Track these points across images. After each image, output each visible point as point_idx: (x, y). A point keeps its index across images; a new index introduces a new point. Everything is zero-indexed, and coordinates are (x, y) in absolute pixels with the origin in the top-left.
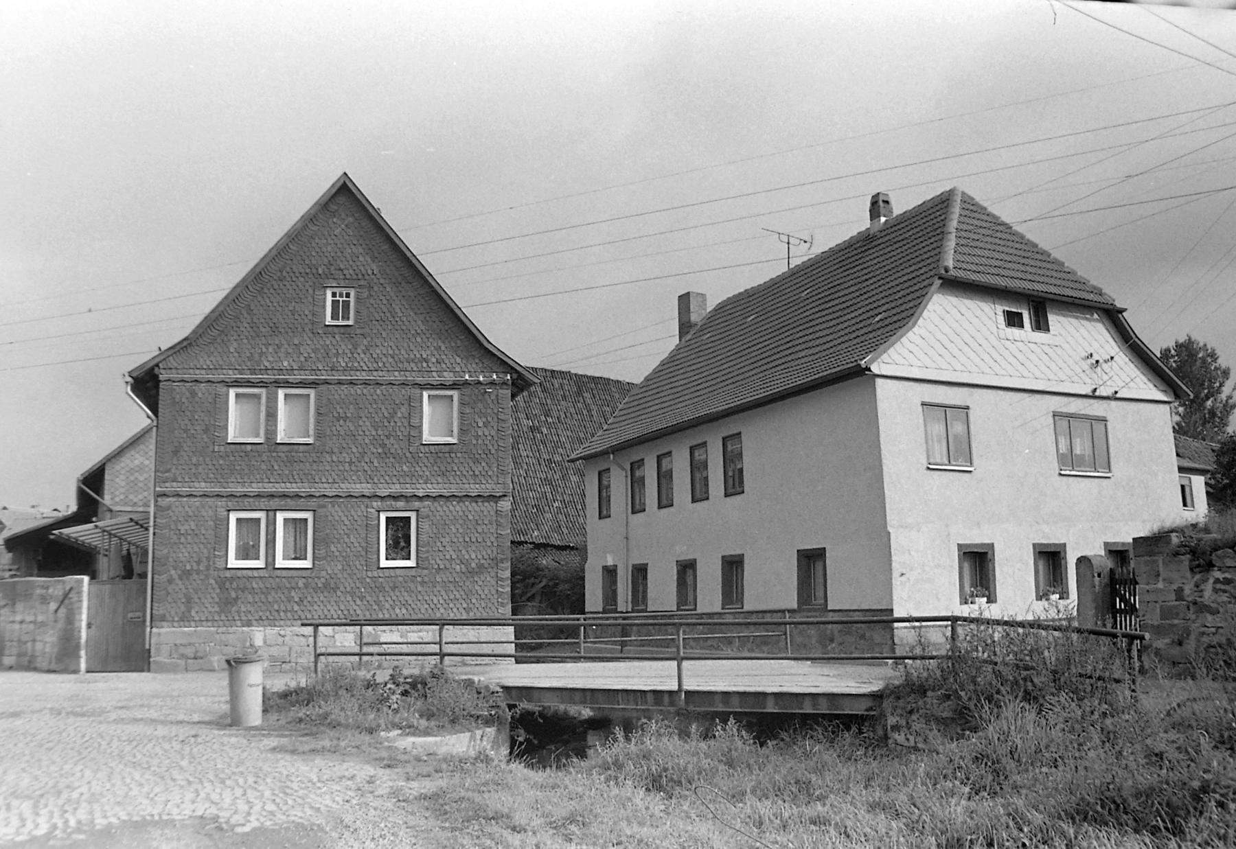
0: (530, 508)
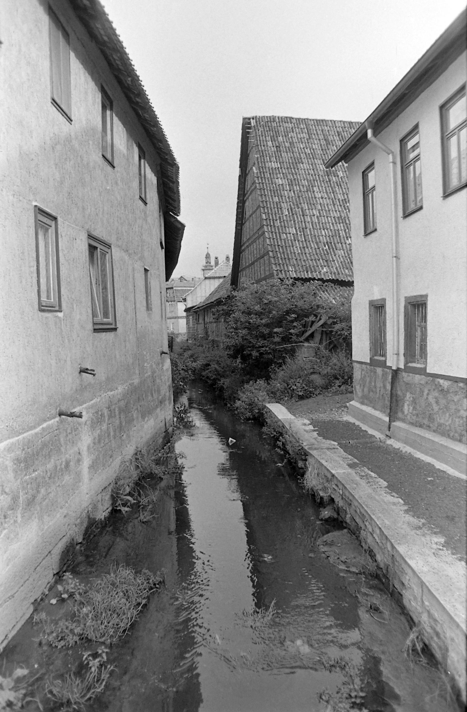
0: (321, 245)
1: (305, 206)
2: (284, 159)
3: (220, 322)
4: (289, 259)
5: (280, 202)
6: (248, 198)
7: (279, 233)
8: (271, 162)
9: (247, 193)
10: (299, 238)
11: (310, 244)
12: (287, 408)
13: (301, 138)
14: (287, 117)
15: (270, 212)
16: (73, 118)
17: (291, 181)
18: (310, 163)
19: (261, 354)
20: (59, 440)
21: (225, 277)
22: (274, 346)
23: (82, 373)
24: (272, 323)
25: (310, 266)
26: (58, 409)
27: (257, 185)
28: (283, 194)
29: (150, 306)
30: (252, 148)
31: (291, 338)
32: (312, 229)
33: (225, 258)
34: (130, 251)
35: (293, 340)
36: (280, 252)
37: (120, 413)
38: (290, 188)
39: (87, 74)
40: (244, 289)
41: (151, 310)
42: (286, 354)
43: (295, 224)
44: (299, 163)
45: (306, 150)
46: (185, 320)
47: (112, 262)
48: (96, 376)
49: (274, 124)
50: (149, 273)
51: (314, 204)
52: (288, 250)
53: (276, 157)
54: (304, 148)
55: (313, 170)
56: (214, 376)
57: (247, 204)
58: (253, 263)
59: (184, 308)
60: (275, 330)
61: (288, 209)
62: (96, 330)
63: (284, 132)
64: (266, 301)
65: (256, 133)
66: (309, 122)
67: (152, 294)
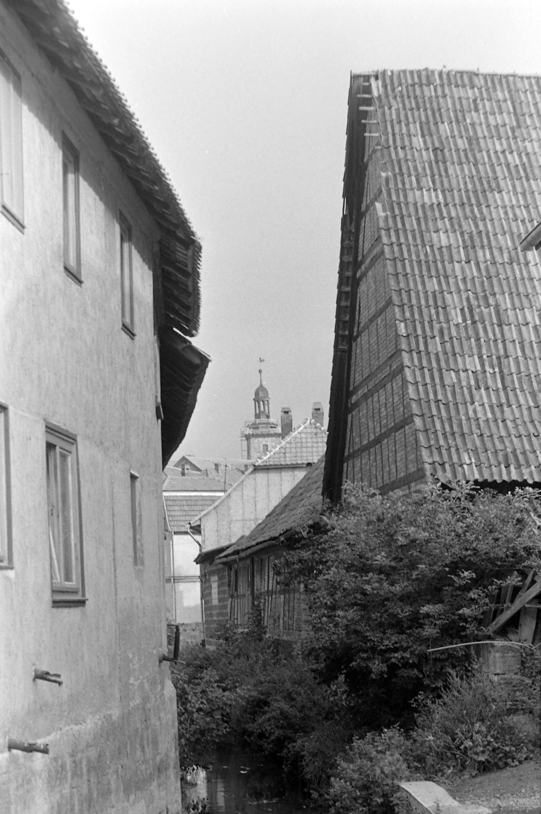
1: (506, 302)
2: (454, 181)
3: (295, 591)
4: (463, 435)
5: (442, 292)
6: (364, 274)
7: (440, 370)
8: (421, 189)
9: (362, 262)
10: (490, 383)
11: (516, 396)
12: (448, 790)
13: (497, 126)
14: (462, 73)
15: (417, 316)
16: (26, 224)
17: (471, 237)
18: (519, 190)
19: (393, 668)
20: (8, 791)
21: (309, 464)
22: (423, 647)
23: (40, 682)
24: (419, 593)
25: (514, 452)
26: (7, 737)
27: (387, 249)
28: (449, 272)
29: (139, 554)
30: (374, 151)
31: (464, 629)
32: (521, 359)
33: (311, 411)
34: (107, 444)
35: (468, 632)
36: (441, 418)
37: (89, 771)
38: (467, 255)
39: (42, 127)
40: (350, 509)
41: (142, 563)
42: (454, 667)
43: (479, 347)
44: (492, 191)
45: (509, 157)
46: (197, 587)
47: (78, 470)
48: (64, 685)
49: (429, 92)
50: (138, 484)
51: (527, 296)
52: (462, 412)
53: (433, 176)
54: (503, 152)
55: (527, 207)
56: (278, 733)
57: (363, 288)
58: (378, 441)
59: (196, 553)
60: (425, 609)
61: (462, 310)
62: (56, 604)
63: (455, 111)
64: (402, 540)
65: (384, 114)
66: (519, 85)
67: (144, 529)
